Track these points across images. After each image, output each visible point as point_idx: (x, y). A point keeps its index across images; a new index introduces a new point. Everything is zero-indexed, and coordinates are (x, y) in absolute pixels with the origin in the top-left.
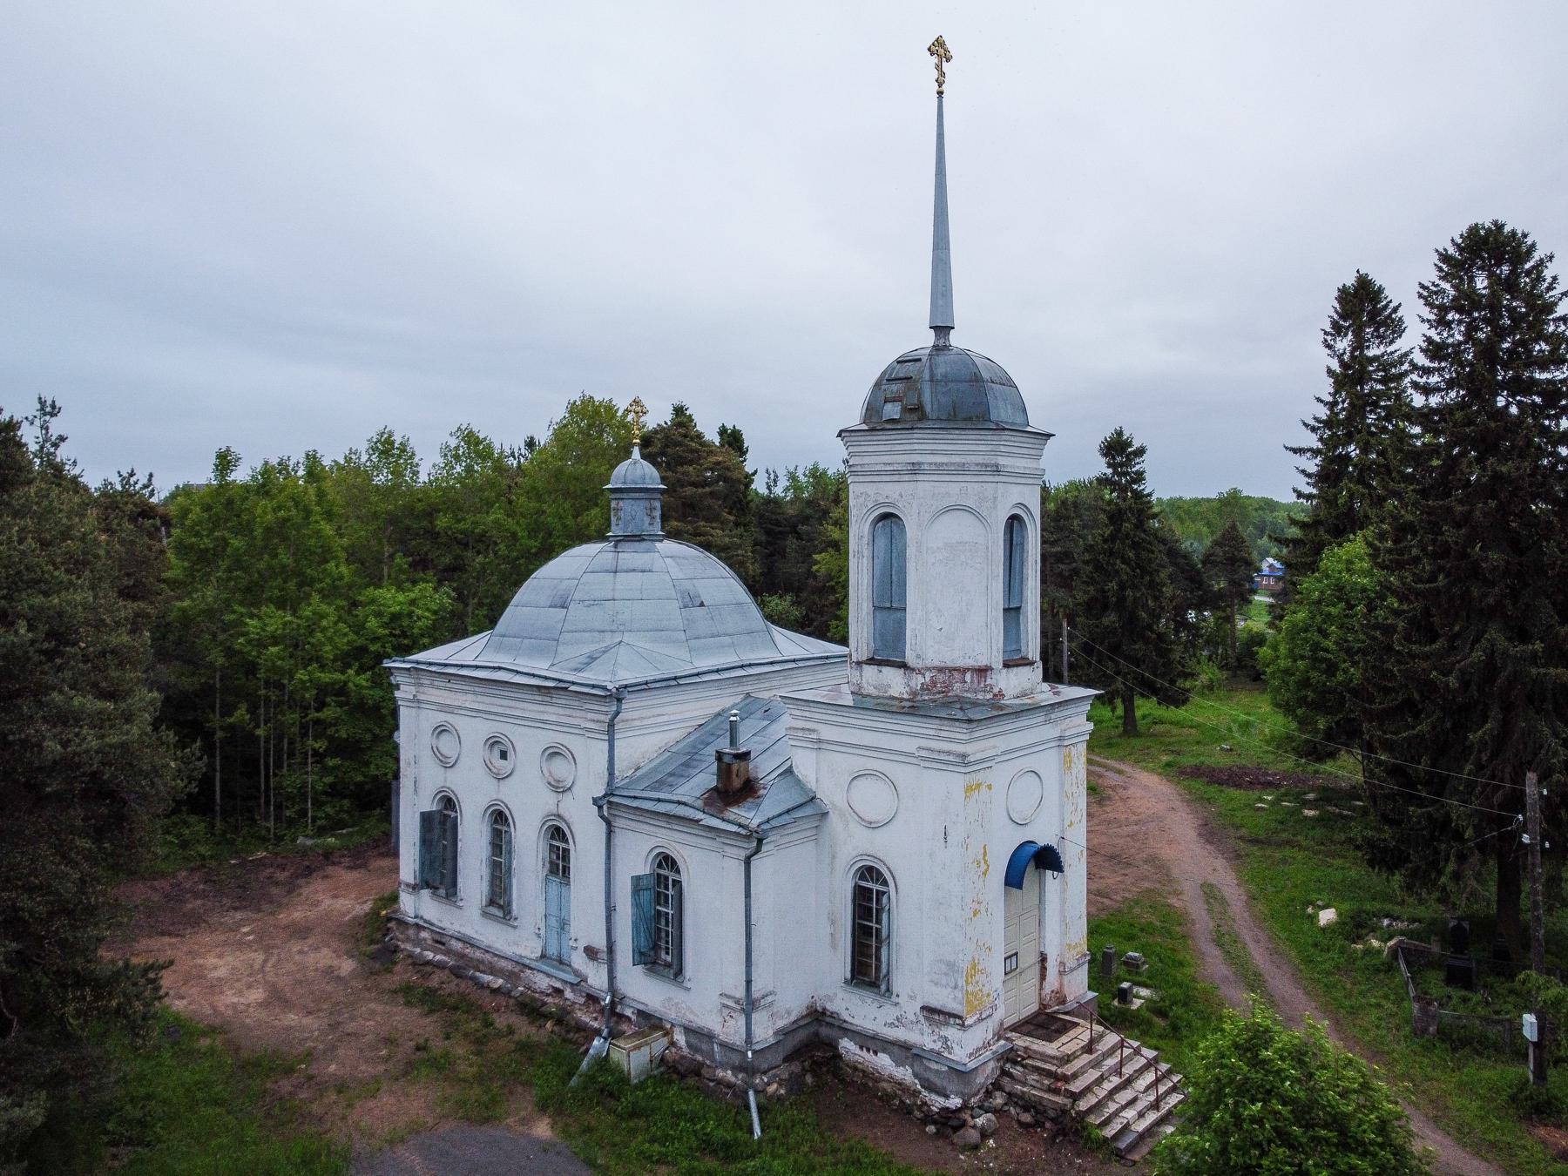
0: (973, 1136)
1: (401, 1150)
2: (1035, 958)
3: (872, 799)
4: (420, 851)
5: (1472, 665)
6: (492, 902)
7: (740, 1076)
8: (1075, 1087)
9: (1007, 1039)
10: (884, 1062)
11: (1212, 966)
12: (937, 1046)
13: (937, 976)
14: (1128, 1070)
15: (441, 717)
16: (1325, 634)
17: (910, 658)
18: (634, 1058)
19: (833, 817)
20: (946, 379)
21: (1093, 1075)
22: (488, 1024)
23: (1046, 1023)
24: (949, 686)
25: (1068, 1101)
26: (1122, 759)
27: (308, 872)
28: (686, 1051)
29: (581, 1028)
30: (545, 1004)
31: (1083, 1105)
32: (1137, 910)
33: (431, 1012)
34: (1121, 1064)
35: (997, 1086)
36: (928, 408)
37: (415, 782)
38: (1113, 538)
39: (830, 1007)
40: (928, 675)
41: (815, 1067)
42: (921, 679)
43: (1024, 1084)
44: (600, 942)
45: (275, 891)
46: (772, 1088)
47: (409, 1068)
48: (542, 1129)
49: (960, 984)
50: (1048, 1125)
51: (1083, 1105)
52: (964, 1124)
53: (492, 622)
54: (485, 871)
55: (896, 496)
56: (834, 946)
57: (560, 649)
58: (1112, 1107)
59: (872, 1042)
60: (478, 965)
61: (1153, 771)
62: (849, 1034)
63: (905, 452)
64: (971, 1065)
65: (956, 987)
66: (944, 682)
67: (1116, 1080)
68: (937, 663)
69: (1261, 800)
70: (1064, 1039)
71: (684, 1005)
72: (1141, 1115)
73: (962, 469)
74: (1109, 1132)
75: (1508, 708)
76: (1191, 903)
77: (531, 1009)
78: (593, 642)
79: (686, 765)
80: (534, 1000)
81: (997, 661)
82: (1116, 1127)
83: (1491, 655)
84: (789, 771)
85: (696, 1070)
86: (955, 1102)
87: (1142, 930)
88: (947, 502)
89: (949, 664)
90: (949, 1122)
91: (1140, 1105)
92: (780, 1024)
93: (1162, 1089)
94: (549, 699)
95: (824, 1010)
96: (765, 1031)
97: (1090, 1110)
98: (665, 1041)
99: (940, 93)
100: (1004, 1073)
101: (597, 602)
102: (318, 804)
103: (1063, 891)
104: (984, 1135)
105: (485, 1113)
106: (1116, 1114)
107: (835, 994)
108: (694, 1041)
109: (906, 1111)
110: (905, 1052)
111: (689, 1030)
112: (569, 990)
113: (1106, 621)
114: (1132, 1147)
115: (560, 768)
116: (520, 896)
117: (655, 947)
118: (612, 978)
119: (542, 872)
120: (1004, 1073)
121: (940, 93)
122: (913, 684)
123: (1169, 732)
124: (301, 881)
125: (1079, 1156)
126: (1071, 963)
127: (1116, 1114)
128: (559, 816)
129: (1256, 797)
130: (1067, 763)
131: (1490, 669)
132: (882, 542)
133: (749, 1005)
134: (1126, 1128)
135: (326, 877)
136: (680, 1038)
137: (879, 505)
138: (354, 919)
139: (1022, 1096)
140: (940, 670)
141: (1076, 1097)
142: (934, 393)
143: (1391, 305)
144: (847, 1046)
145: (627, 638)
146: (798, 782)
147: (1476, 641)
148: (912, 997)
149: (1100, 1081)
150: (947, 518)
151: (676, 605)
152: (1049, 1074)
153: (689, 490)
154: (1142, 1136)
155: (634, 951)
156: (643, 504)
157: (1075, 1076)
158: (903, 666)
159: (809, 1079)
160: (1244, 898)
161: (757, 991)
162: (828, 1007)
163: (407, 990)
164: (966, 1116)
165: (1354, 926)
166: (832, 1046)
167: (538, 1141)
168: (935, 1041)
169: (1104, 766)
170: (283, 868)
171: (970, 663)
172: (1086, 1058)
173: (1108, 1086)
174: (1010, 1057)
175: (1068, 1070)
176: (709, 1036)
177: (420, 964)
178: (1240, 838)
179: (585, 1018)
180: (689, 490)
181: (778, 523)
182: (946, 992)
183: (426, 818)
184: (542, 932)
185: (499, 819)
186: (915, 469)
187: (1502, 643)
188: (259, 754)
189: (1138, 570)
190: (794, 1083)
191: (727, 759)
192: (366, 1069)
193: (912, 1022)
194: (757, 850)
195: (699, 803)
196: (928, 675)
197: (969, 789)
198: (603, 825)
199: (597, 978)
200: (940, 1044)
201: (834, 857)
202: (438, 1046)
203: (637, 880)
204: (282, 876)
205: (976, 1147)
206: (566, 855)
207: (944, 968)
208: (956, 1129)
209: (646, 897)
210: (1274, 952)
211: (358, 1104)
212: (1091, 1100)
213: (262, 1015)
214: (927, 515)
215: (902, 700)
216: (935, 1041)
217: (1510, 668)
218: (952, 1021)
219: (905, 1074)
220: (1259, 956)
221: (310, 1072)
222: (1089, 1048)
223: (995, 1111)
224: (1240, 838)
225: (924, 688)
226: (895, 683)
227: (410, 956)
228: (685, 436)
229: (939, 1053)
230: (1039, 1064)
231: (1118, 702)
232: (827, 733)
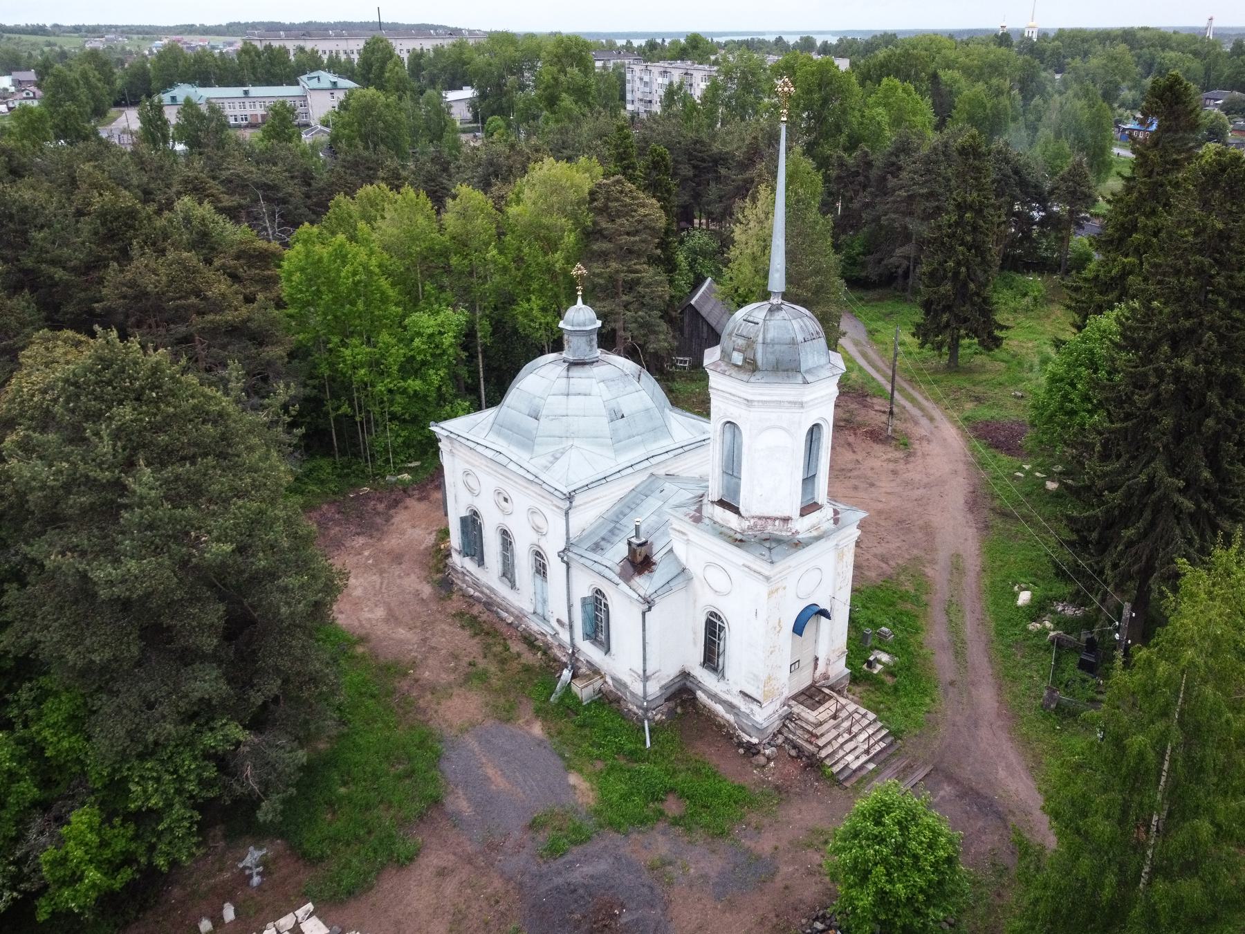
0: (762, 760)
1: (466, 736)
2: (811, 659)
5: (1137, 484)
6: (504, 575)
8: (821, 742)
9: (789, 706)
10: (719, 709)
11: (934, 635)
12: (748, 711)
14: (855, 729)
15: (468, 467)
16: (1073, 385)
17: (742, 510)
18: (583, 691)
19: (695, 581)
20: (773, 343)
21: (834, 733)
22: (507, 649)
23: (812, 695)
24: (764, 528)
25: (816, 750)
26: (937, 401)
27: (395, 503)
28: (612, 688)
29: (556, 660)
30: (536, 639)
31: (823, 754)
32: (902, 578)
33: (476, 634)
34: (852, 726)
35: (780, 732)
36: (759, 363)
38: (957, 224)
40: (752, 521)
41: (683, 703)
42: (747, 523)
43: (794, 734)
44: (565, 620)
45: (378, 520)
46: (657, 718)
47: (468, 678)
48: (537, 729)
51: (823, 754)
52: (759, 752)
53: (495, 398)
54: (500, 559)
56: (695, 644)
58: (841, 753)
59: (714, 697)
60: (499, 605)
61: (954, 422)
64: (765, 725)
67: (847, 736)
68: (758, 514)
69: (1020, 469)
70: (821, 709)
72: (857, 758)
73: (779, 403)
74: (835, 769)
75: (1156, 512)
76: (937, 574)
77: (529, 640)
79: (612, 532)
80: (531, 634)
81: (795, 513)
82: (840, 766)
83: (1151, 479)
84: (671, 550)
85: (618, 700)
86: (755, 740)
87: (901, 598)
89: (766, 515)
90: (751, 750)
91: (857, 753)
92: (663, 682)
93: (872, 742)
95: (689, 674)
96: (654, 689)
97: (827, 757)
98: (601, 681)
100: (784, 725)
101: (557, 417)
102: (395, 453)
103: (832, 629)
104: (769, 759)
105: (506, 715)
106: (843, 757)
109: (730, 737)
110: (731, 707)
111: (613, 679)
113: (942, 290)
114: (846, 779)
117: (595, 632)
118: (572, 639)
119: (532, 571)
120: (784, 725)
123: (983, 366)
124: (392, 512)
125: (817, 780)
126: (833, 658)
127: (843, 757)
129: (1018, 464)
130: (840, 556)
131: (1150, 487)
132: (728, 436)
133: (646, 678)
134: (847, 766)
135: (406, 508)
136: (610, 682)
138: (426, 549)
139: (792, 741)
140: (760, 518)
141: (820, 748)
142: (764, 353)
144: (699, 694)
145: (576, 442)
146: (676, 559)
147: (1145, 466)
149: (836, 738)
151: (605, 420)
152: (808, 732)
153: (625, 239)
154: (855, 771)
156: (584, 339)
157: (822, 735)
158: (736, 510)
159: (679, 710)
160: (978, 569)
161: (648, 673)
163: (460, 615)
164: (761, 748)
165: (1038, 609)
166: (693, 693)
167: (534, 738)
169: (922, 409)
170: (380, 500)
171: (779, 514)
172: (832, 722)
173: (841, 740)
174: (789, 717)
175: (818, 731)
176: (625, 686)
177: (465, 596)
178: (993, 509)
179: (559, 653)
180: (625, 239)
181: (703, 160)
183: (464, 521)
185: (506, 538)
187: (1162, 473)
189: (963, 269)
190: (671, 713)
191: (634, 546)
192: (445, 678)
194: (650, 609)
195: (618, 569)
196: (752, 521)
197: (771, 593)
198: (564, 565)
199: (565, 636)
201: (695, 601)
202: (482, 663)
203: (584, 600)
204: (381, 507)
205: (764, 766)
206: (544, 566)
208: (754, 754)
209: (590, 608)
210: (982, 622)
211: (443, 702)
212: (829, 750)
213: (385, 628)
215: (736, 532)
217: (1162, 490)
219: (730, 718)
220: (969, 628)
221: (417, 676)
222: (834, 717)
223: (776, 746)
224: (993, 509)
225: (750, 528)
227: (461, 589)
228: (621, 192)
230: (804, 725)
231: (945, 349)
232: (692, 537)
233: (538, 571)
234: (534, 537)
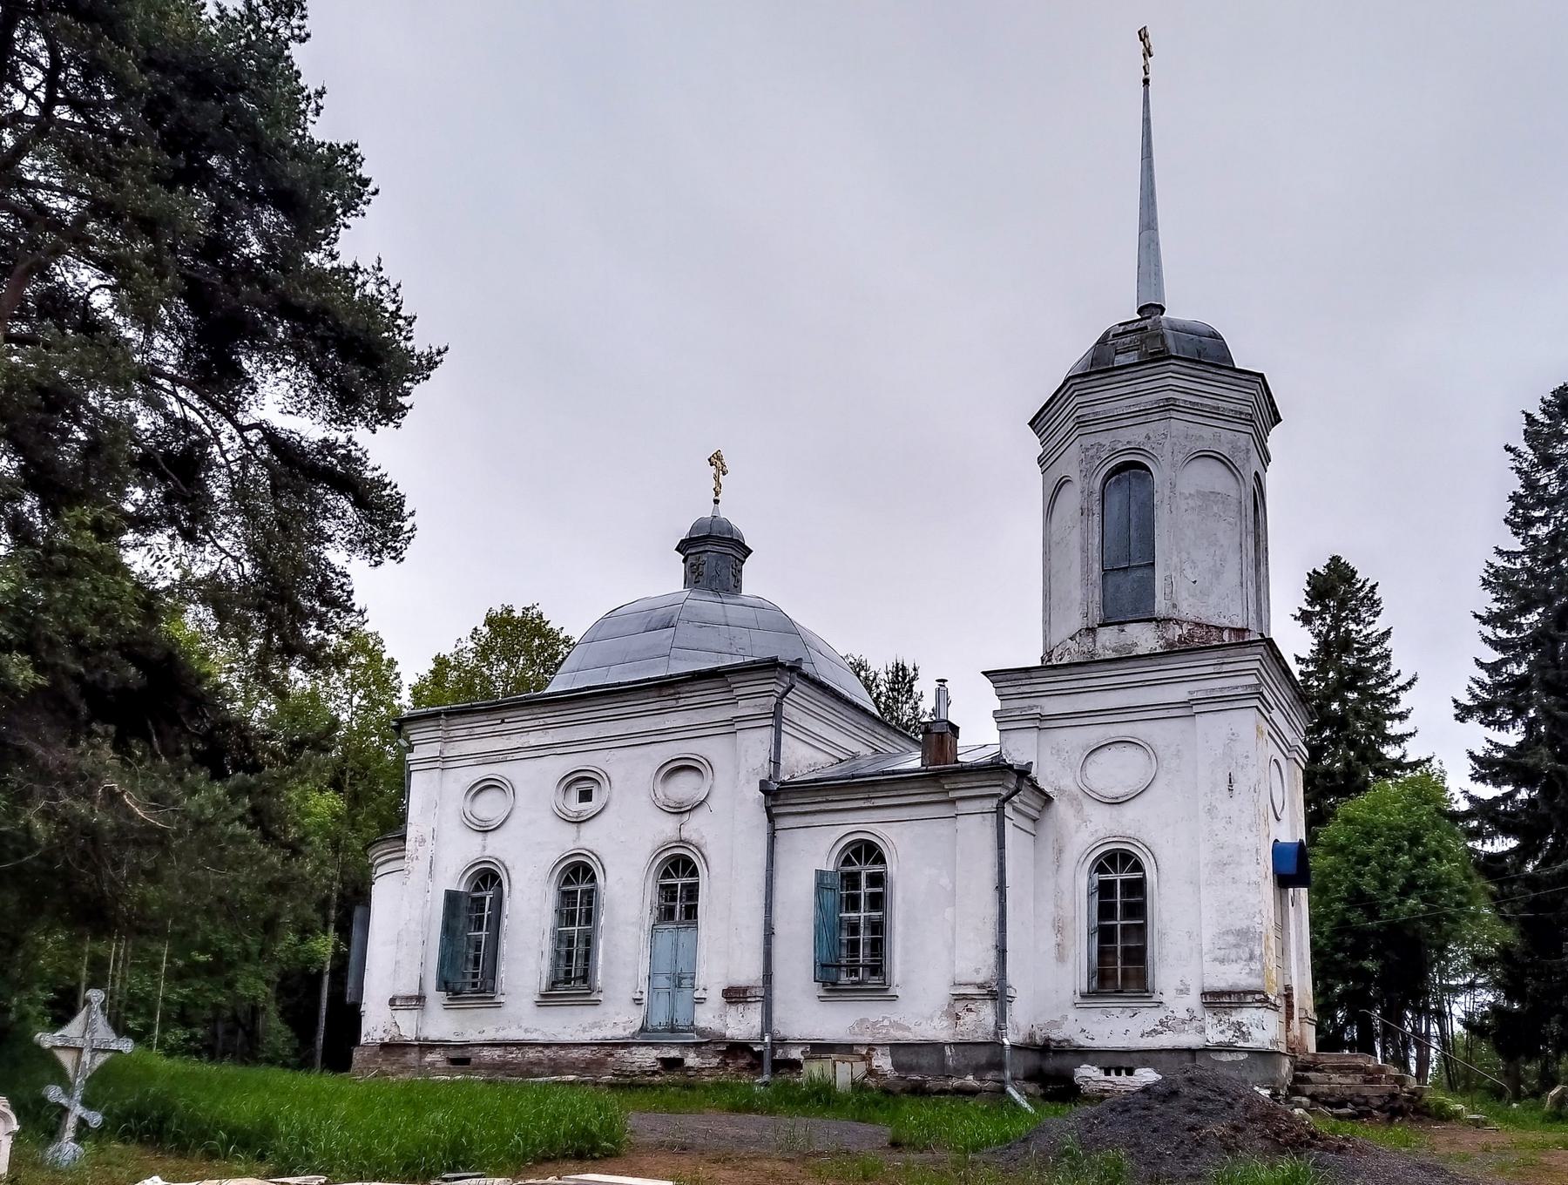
3: (1117, 771)
4: (441, 945)
7: (989, 1077)
12: (1228, 1036)
13: (1223, 952)
19: (1061, 807)
37: (431, 863)
39: (1056, 1035)
49: (1257, 953)
50: (1375, 1112)
55: (1142, 439)
57: (672, 662)
62: (1091, 1057)
63: (1155, 391)
65: (1251, 958)
66: (1202, 638)
68: (1191, 617)
71: (886, 1023)
73: (1215, 413)
78: (710, 661)
88: (1199, 446)
94: (673, 703)
99: (1146, 82)
107: (1065, 1017)
108: (905, 1058)
111: (896, 1047)
112: (692, 1055)
115: (684, 787)
116: (608, 961)
121: (1146, 82)
122: (1169, 635)
128: (681, 841)
136: (883, 1062)
137: (1117, 452)
143: (1369, 584)
148: (1183, 991)
150: (1198, 464)
155: (815, 963)
162: (1052, 1036)
168: (1222, 1032)
182: (1236, 967)
184: (645, 996)
186: (1168, 406)
188: (110, 954)
193: (1184, 1022)
200: (1230, 1034)
201: (1060, 851)
206: (692, 891)
207: (1231, 939)
209: (830, 898)
214: (1181, 456)
216: (1222, 1032)
218: (1249, 998)
226: (1144, 638)
229: (1230, 1044)
232: (1052, 706)
233: (667, 914)
234: (667, 828)
